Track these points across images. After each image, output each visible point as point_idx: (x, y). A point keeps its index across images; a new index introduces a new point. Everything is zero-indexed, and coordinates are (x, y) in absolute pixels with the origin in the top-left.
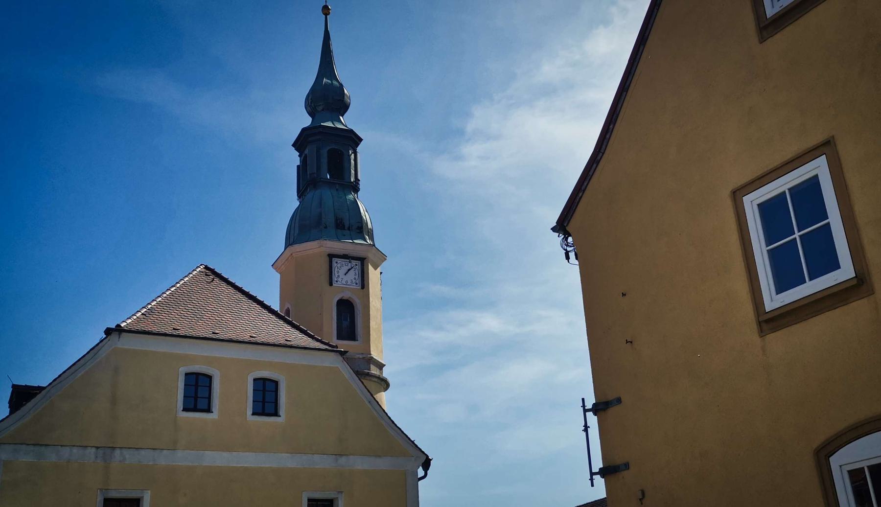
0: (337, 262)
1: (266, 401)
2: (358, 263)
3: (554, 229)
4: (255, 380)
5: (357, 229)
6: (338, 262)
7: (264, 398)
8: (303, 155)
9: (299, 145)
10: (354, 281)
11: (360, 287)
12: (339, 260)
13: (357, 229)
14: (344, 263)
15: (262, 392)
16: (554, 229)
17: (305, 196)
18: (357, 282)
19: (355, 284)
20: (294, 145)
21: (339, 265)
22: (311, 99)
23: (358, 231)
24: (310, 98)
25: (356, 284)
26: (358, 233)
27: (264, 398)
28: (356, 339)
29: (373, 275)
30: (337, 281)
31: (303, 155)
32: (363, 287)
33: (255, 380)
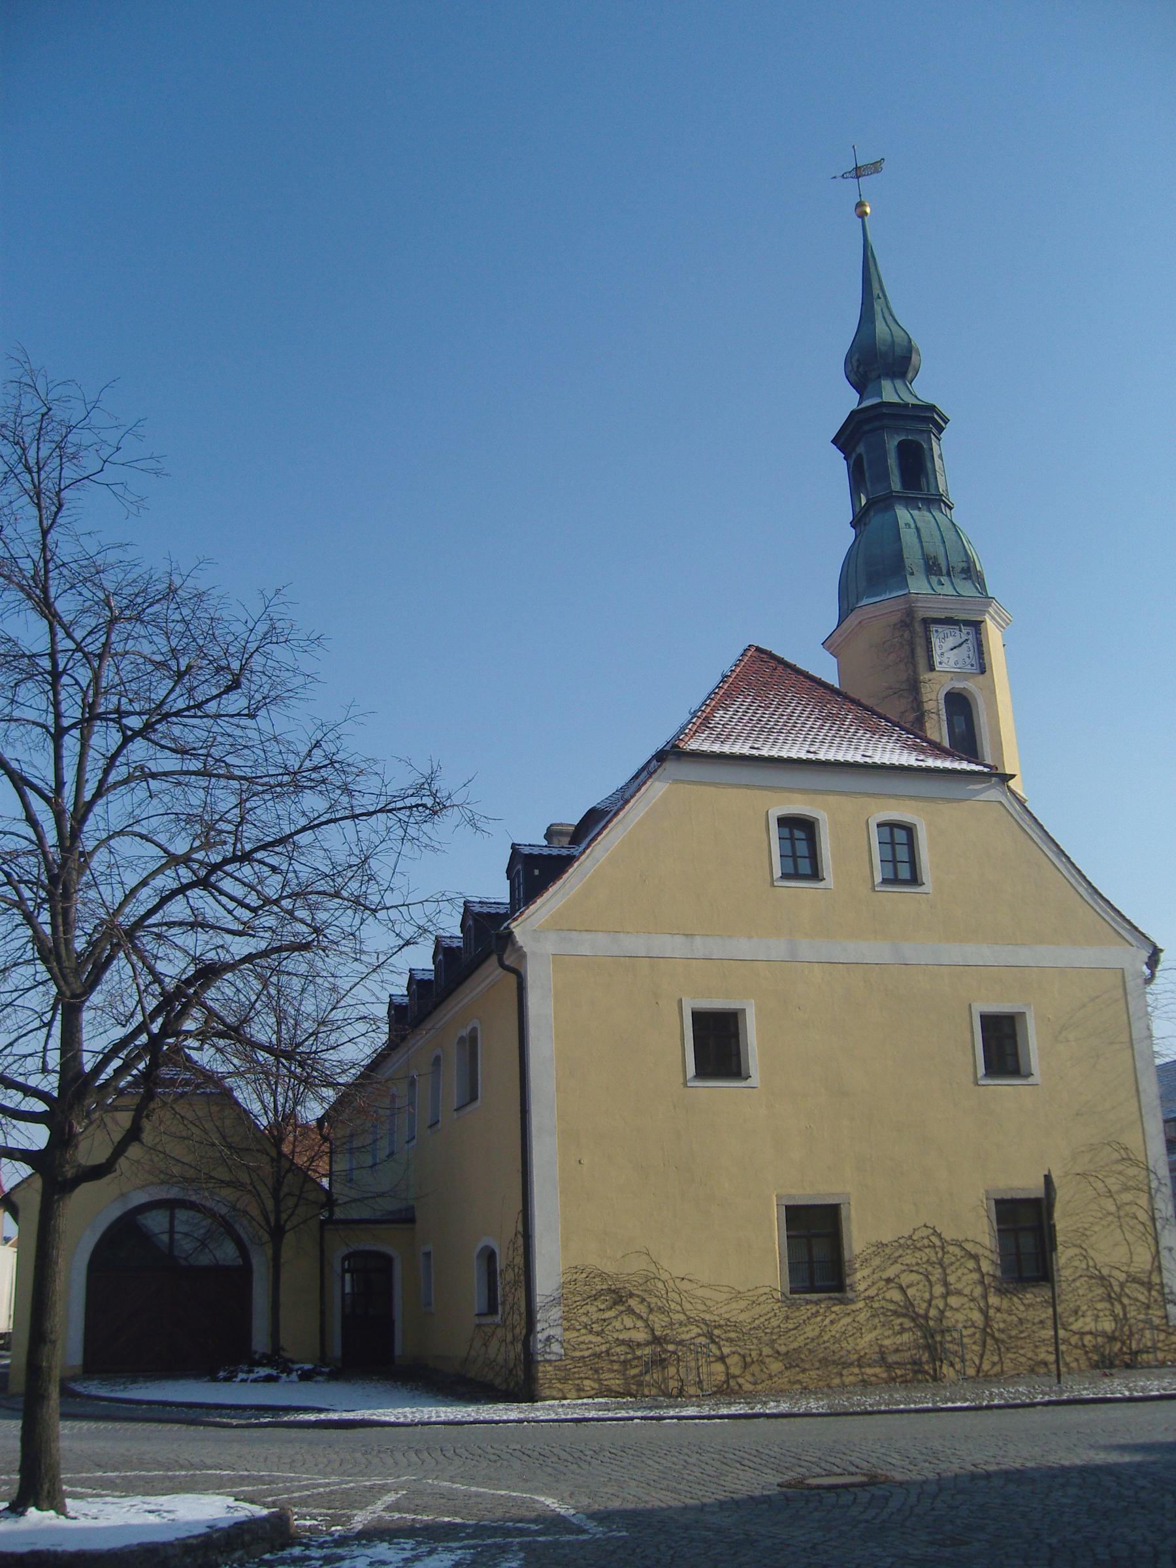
0: (937, 631)
1: (808, 860)
2: (970, 630)
3: (1161, 951)
4: (879, 825)
5: (961, 573)
6: (940, 630)
7: (894, 851)
8: (854, 456)
9: (845, 440)
10: (967, 660)
11: (978, 671)
12: (940, 628)
13: (961, 573)
14: (948, 631)
15: (807, 860)
16: (1161, 951)
17: (865, 524)
18: (973, 662)
19: (969, 667)
20: (834, 441)
21: (941, 635)
22: (858, 360)
23: (964, 576)
24: (856, 357)
25: (972, 665)
26: (964, 579)
27: (894, 851)
28: (1023, 1070)
29: (994, 635)
30: (940, 663)
31: (854, 456)
32: (983, 671)
33: (879, 825)
